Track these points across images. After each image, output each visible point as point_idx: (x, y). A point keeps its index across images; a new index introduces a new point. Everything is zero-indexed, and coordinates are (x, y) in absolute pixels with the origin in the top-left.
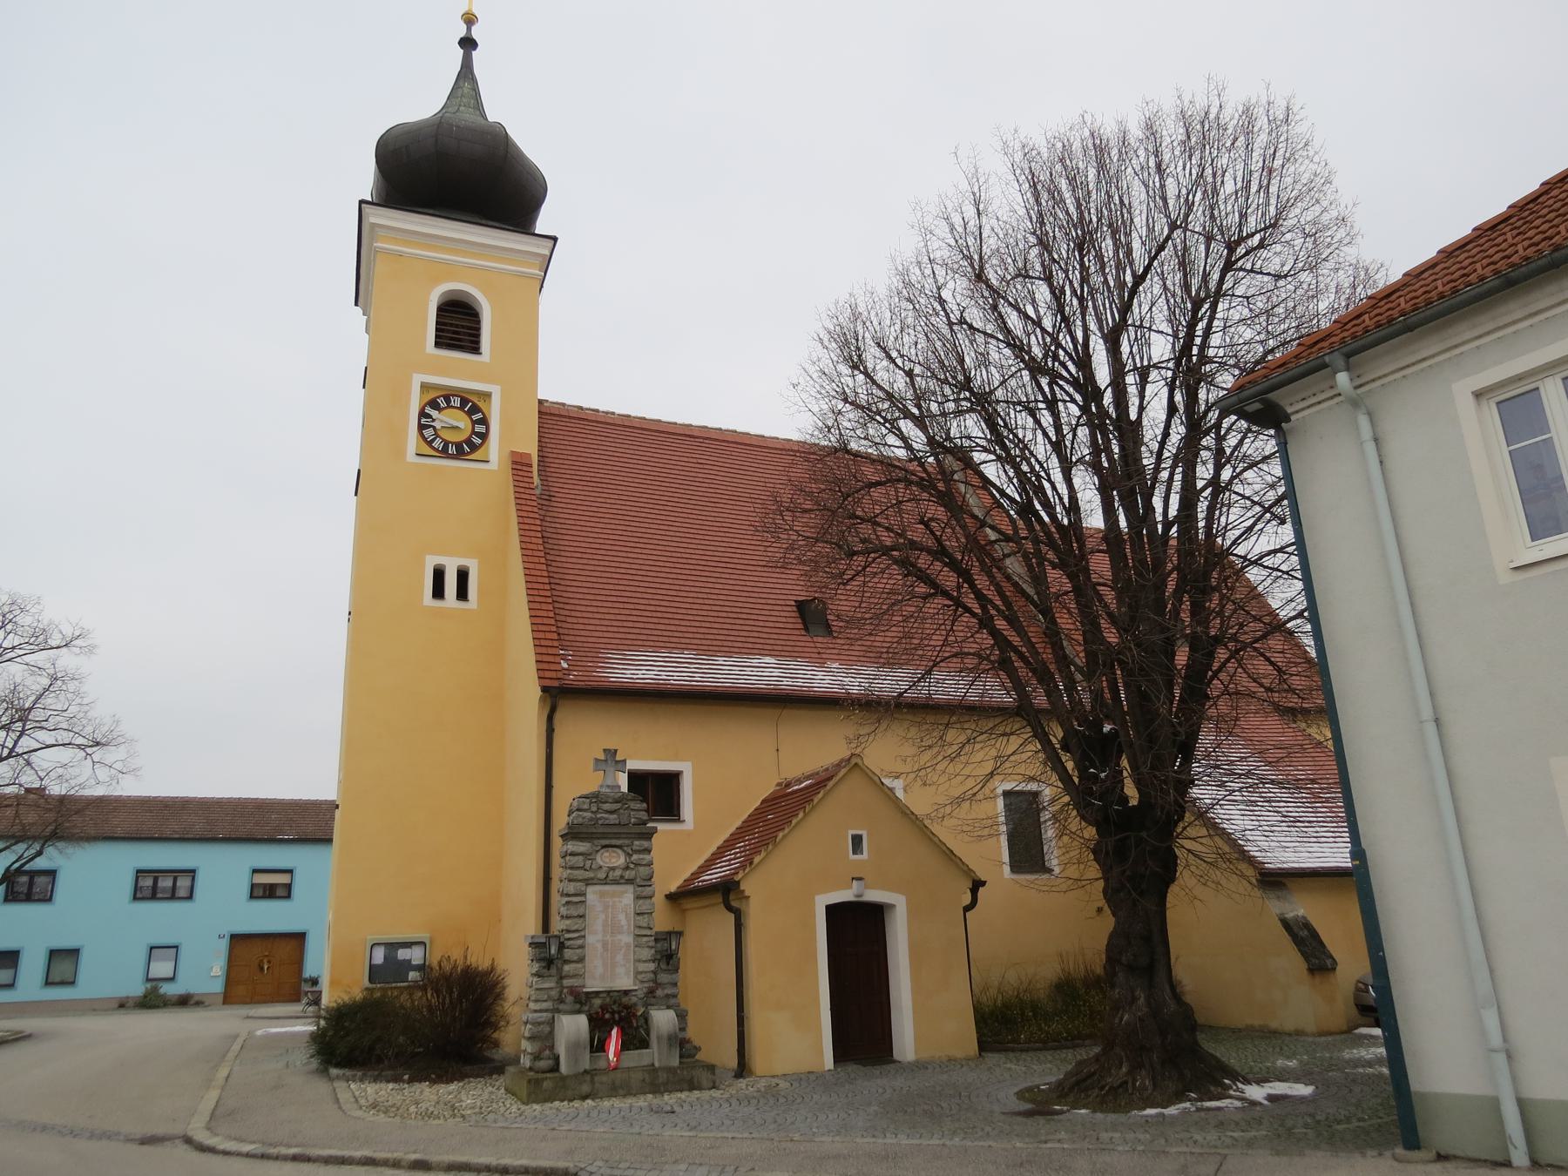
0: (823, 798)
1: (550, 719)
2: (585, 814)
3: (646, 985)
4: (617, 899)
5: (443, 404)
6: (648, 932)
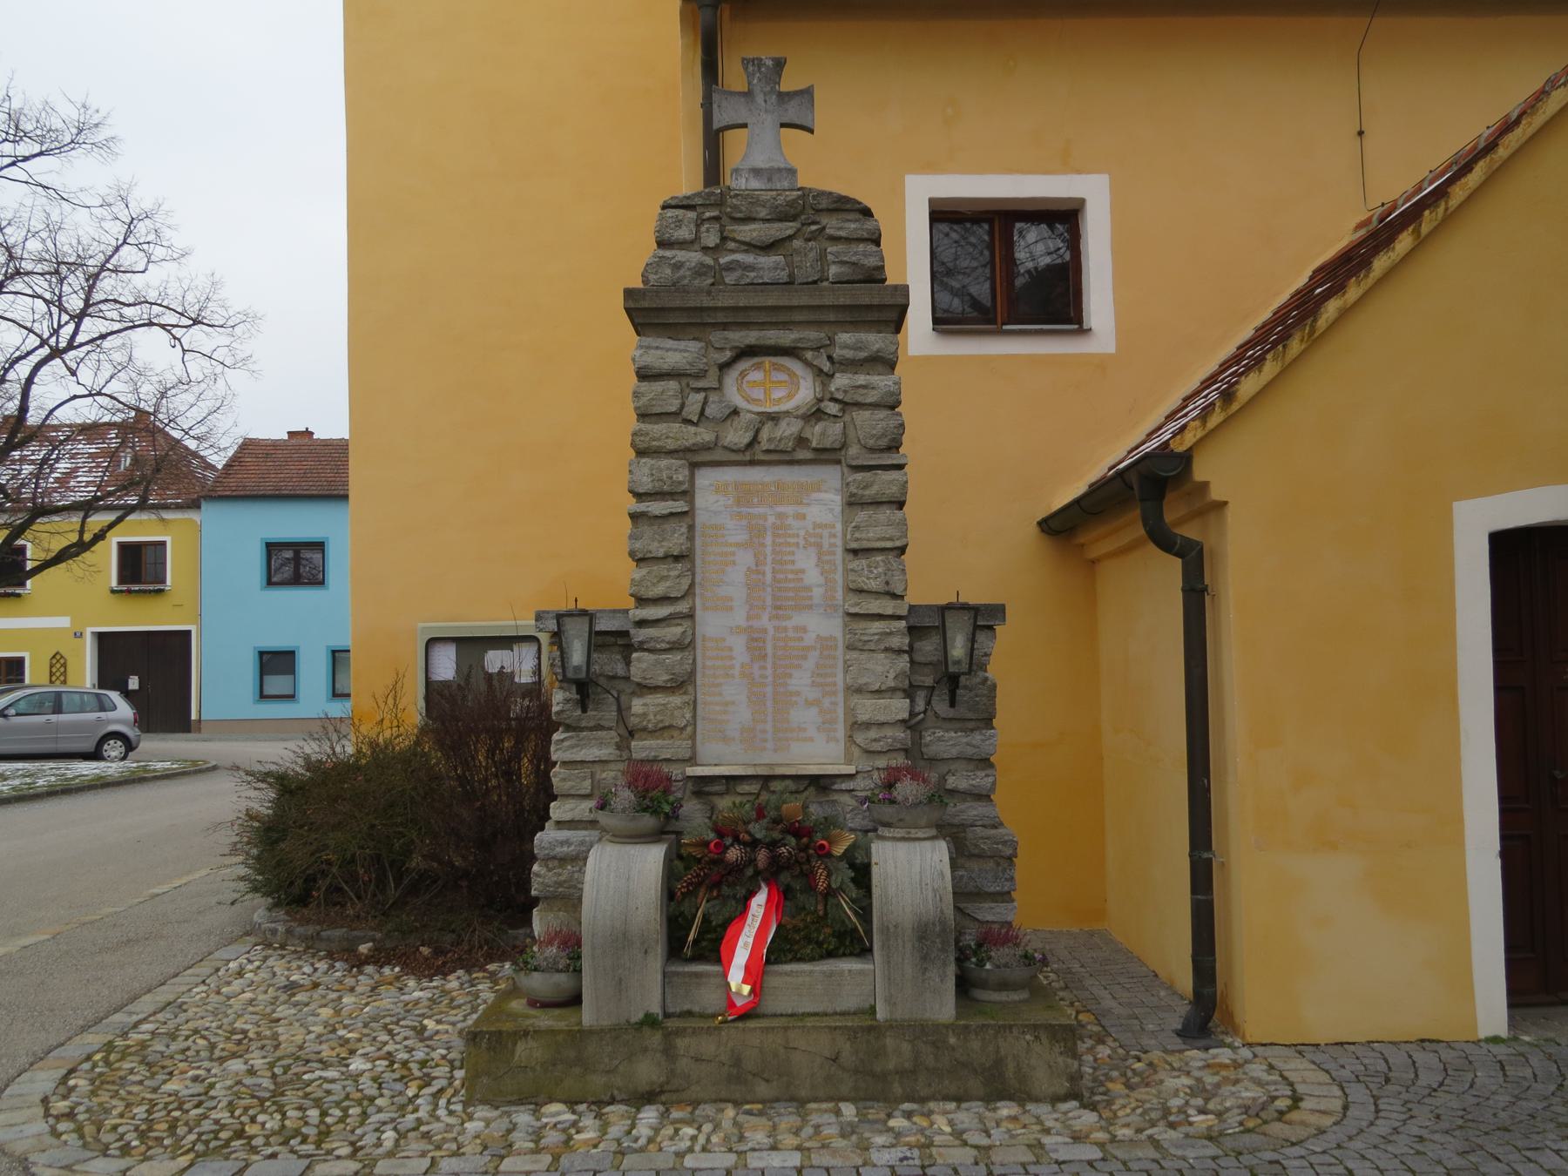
2: (680, 255)
3: (881, 762)
4: (789, 510)
6: (888, 607)
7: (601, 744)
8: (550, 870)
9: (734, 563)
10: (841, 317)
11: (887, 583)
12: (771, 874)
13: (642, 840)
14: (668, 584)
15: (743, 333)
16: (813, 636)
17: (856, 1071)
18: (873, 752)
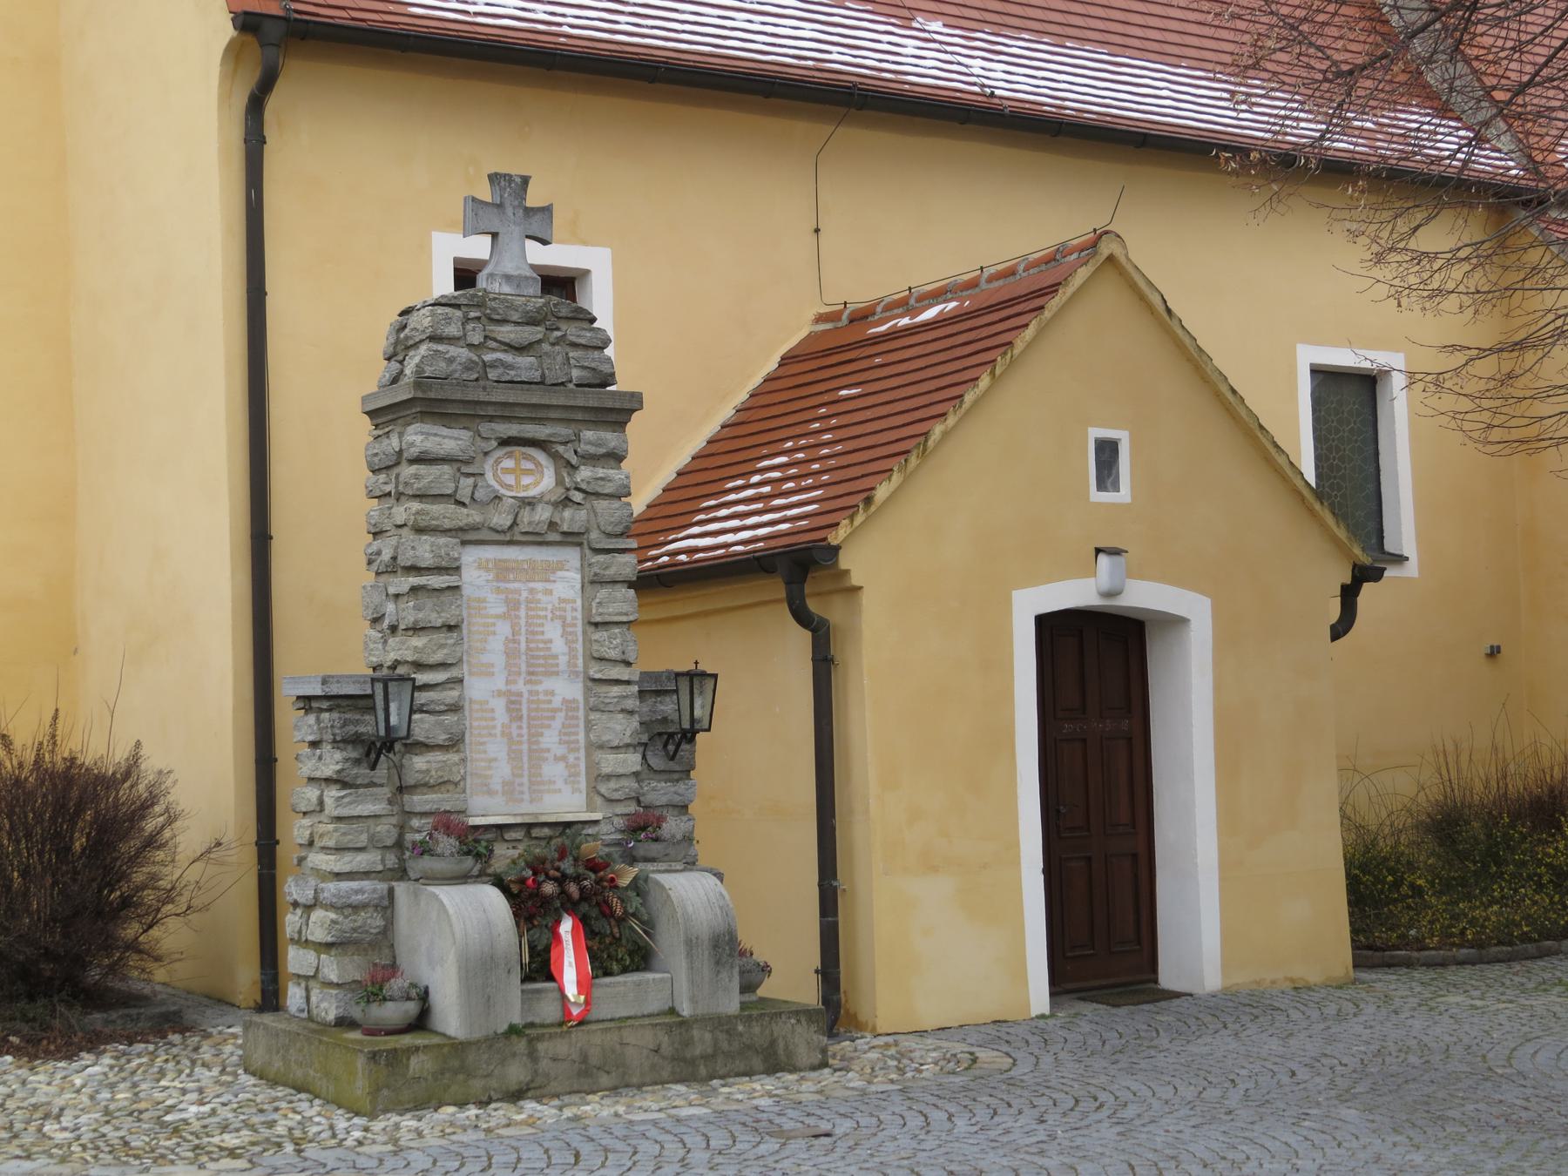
0: (1035, 339)
1: (256, 106)
2: (453, 351)
4: (539, 586)
7: (376, 799)
8: (346, 917)
9: (494, 633)
10: (587, 417)
11: (623, 653)
12: (570, 906)
13: (460, 881)
14: (445, 651)
15: (507, 426)
17: (673, 1059)
18: (612, 801)
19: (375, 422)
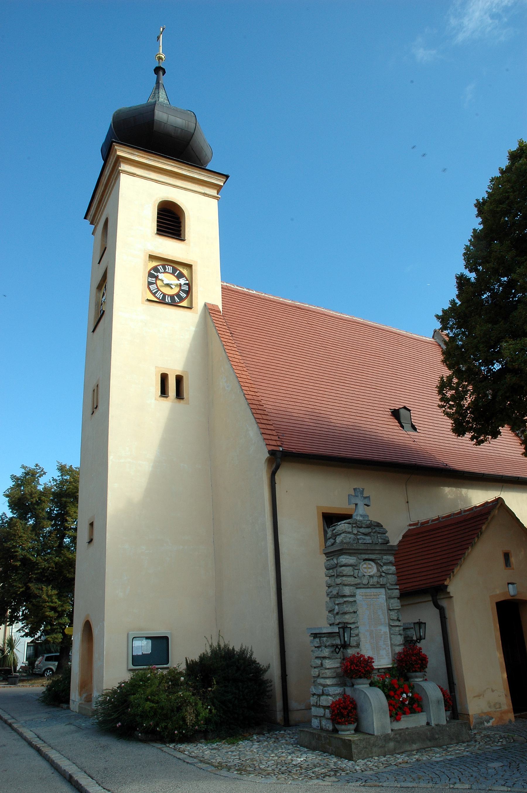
5: (162, 270)
6: (397, 623)
16: (383, 631)
19: (327, 556)
